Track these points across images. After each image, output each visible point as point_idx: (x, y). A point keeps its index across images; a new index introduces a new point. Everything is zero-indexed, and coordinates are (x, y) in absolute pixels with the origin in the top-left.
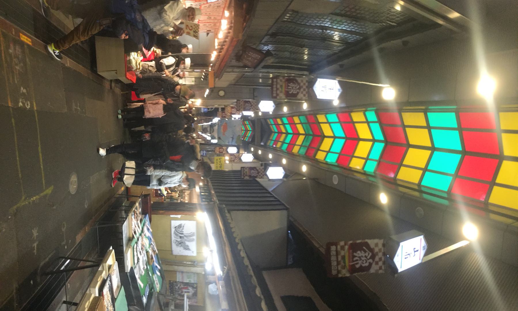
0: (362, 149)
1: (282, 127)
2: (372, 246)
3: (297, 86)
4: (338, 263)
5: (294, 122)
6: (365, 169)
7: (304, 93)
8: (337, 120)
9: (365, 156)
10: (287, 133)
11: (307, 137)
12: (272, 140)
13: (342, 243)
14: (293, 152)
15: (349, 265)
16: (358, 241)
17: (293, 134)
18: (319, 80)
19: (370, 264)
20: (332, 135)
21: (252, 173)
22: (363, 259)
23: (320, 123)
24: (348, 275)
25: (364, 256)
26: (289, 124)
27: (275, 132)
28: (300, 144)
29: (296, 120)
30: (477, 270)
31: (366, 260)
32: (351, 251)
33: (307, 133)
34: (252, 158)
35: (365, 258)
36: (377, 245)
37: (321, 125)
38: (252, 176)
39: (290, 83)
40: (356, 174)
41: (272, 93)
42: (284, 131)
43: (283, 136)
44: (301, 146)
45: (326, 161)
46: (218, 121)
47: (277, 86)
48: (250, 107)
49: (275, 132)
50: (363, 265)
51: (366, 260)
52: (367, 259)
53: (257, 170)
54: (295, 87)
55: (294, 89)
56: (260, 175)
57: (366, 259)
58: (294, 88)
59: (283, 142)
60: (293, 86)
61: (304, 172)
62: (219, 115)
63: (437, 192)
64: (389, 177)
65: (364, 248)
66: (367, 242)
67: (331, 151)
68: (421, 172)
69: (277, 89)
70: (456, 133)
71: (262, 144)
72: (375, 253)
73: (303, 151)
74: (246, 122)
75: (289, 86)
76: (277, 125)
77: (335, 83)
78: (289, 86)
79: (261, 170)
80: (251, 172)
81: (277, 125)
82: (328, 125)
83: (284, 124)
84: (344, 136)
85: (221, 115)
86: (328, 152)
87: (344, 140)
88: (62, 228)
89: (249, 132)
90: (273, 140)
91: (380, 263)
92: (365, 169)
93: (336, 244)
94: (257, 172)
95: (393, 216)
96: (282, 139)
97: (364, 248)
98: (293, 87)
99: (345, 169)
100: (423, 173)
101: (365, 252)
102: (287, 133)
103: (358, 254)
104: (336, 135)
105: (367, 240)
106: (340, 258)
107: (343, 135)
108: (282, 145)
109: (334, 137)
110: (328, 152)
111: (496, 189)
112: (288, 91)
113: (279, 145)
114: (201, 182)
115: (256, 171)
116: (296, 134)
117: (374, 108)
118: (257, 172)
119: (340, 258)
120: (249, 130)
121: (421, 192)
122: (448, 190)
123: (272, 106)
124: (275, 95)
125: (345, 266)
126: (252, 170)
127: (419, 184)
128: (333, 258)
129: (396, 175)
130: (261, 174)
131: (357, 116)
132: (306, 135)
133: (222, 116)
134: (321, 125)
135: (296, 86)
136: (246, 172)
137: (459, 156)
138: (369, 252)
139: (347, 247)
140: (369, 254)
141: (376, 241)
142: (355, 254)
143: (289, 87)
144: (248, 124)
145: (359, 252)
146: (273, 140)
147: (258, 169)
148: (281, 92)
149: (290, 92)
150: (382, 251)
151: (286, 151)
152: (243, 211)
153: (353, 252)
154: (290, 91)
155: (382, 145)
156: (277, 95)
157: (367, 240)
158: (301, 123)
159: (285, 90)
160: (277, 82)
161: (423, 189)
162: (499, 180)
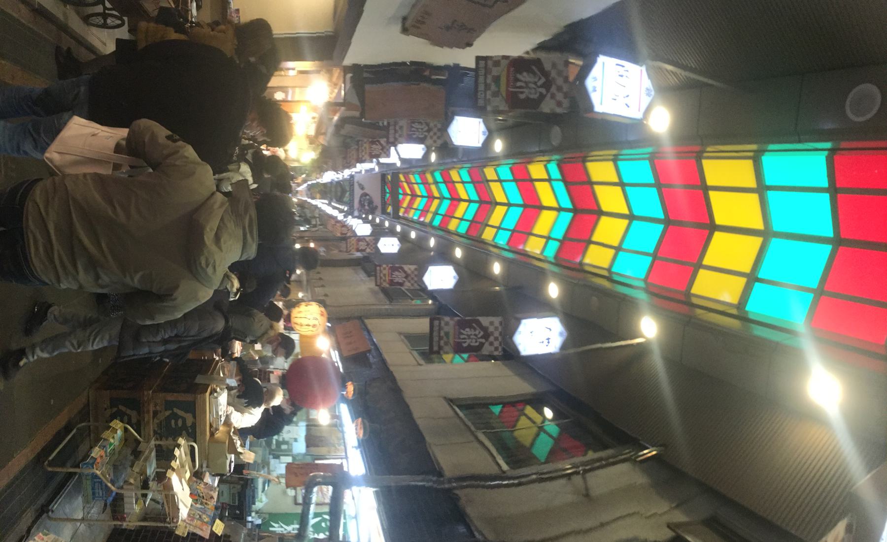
0: (545, 223)
1: (433, 187)
4: (440, 338)
5: (529, 175)
6: (545, 254)
7: (435, 138)
8: (512, 178)
9: (616, 243)
10: (442, 198)
12: (403, 207)
13: (384, 266)
15: (455, 341)
16: (397, 265)
18: (602, 59)
19: (482, 344)
20: (626, 211)
21: (466, 337)
22: (472, 337)
23: (488, 181)
24: (388, 286)
26: (445, 182)
27: (408, 195)
29: (490, 173)
30: (840, 471)
32: (390, 271)
34: (454, 277)
35: (475, 337)
37: (653, 182)
38: (395, 281)
39: (521, 73)
40: (699, 311)
41: (476, 99)
42: (436, 194)
43: (436, 202)
47: (439, 333)
48: (426, 134)
49: (348, 191)
50: (472, 344)
53: (546, 74)
54: (422, 129)
56: (553, 96)
59: (436, 213)
61: (497, 275)
62: (350, 157)
63: (706, 301)
64: (520, 249)
65: (474, 325)
66: (478, 320)
68: (743, 281)
69: (396, 131)
70: (654, 191)
74: (414, 177)
75: (413, 127)
77: (480, 122)
79: (496, 328)
80: (517, 80)
82: (498, 184)
83: (436, 183)
84: (661, 216)
85: (368, 151)
86: (618, 249)
87: (521, 210)
89: (498, 207)
90: (419, 210)
91: (496, 344)
92: (545, 254)
93: (380, 266)
94: (404, 275)
96: (433, 208)
97: (474, 325)
99: (477, 241)
102: (442, 198)
104: (512, 202)
106: (442, 334)
107: (521, 202)
108: (433, 219)
111: (702, 273)
112: (516, 92)
115: (403, 273)
116: (456, 200)
117: (469, 165)
118: (404, 275)
119: (442, 334)
120: (419, 194)
121: (609, 279)
122: (740, 303)
123: (421, 150)
124: (481, 102)
127: (609, 270)
129: (425, 219)
130: (496, 339)
131: (536, 170)
133: (370, 153)
136: (447, 334)
137: (660, 227)
140: (480, 333)
141: (491, 319)
142: (519, 76)
144: (419, 181)
146: (419, 210)
148: (496, 94)
149: (522, 96)
150: (500, 330)
151: (506, 247)
152: (409, 404)
154: (465, 342)
155: (520, 210)
157: (403, 266)
159: (507, 90)
161: (695, 301)
162: (706, 261)
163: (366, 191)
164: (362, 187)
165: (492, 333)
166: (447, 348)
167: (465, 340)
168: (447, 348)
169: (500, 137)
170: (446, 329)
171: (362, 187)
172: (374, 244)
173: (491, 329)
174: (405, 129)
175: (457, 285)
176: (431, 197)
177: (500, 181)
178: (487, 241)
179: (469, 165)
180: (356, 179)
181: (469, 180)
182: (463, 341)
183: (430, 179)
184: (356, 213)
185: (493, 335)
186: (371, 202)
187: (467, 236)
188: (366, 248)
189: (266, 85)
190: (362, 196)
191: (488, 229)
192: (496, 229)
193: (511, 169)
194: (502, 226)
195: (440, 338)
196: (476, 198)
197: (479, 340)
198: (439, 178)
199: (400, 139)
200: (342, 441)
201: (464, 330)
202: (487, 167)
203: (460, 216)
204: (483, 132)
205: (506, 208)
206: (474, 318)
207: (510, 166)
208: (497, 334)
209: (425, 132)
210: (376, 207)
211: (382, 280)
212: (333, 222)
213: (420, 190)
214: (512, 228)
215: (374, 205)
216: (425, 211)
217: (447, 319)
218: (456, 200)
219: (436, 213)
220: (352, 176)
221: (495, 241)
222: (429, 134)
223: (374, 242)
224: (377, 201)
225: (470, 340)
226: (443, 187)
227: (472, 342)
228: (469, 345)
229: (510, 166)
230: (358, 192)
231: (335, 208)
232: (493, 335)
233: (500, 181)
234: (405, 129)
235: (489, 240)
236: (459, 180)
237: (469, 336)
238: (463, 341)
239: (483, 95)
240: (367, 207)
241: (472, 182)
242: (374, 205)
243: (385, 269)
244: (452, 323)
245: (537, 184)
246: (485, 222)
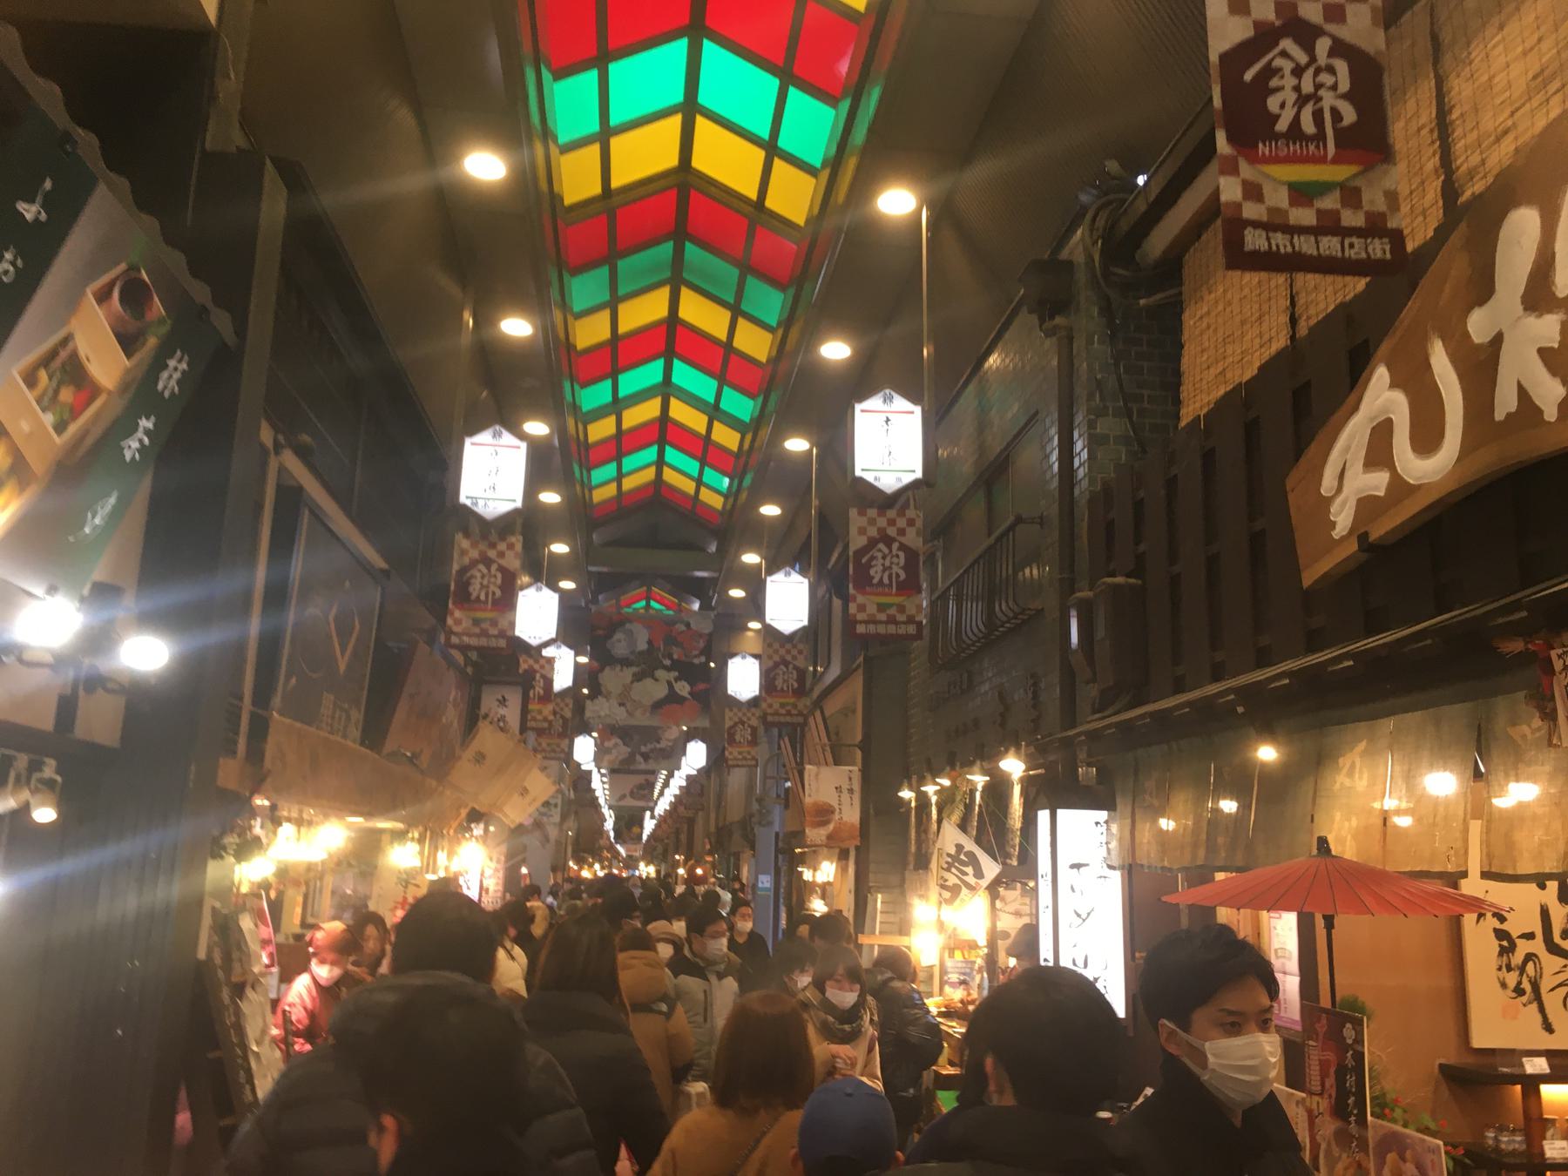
2: (731, 723)
3: (480, 571)
8: (592, 76)
10: (666, 389)
11: (685, 275)
14: (751, 419)
17: (669, 355)
20: (676, 121)
25: (1294, 81)
28: (725, 316)
31: (1317, 72)
32: (1263, 149)
33: (667, 274)
35: (888, 558)
36: (731, 719)
37: (616, 183)
43: (680, 412)
44: (736, 311)
45: (825, 164)
46: (601, 681)
47: (881, 622)
50: (1345, 85)
51: (1317, 72)
52: (1308, 66)
53: (776, 665)
54: (483, 577)
55: (489, 582)
56: (902, 532)
57: (1311, 71)
58: (485, 582)
59: (714, 412)
60: (478, 586)
65: (864, 561)
67: (765, 134)
71: (713, 548)
72: (1278, 23)
73: (769, 302)
75: (478, 597)
76: (622, 444)
78: (478, 597)
79: (872, 522)
81: (622, 444)
82: (616, 143)
83: (617, 405)
84: (680, 47)
86: (771, 148)
87: (709, 48)
88: (455, 825)
89: (698, 163)
90: (701, 473)
95: (965, 157)
96: (696, 421)
97: (864, 561)
98: (481, 584)
100: (705, 403)
101: (873, 558)
102: (666, 389)
103: (1283, 106)
104: (678, 96)
105: (1214, 57)
106: (883, 617)
108: (733, 422)
109: (690, 109)
110: (771, 148)
113: (726, 437)
114: (1256, 750)
119: (883, 617)
125: (1342, 186)
126: (1273, 103)
128: (881, 629)
130: (892, 522)
132: (676, 280)
134: (616, 183)
135: (479, 575)
136: (881, 608)
138: (1276, 51)
139: (1246, 170)
143: (483, 597)
145: (872, 572)
146: (701, 473)
147: (770, 664)
151: (845, 105)
153: (776, 690)
156: (545, 719)
157: (1214, 57)
158: (613, 305)
159: (491, 610)
160: (866, 622)
163: (627, 792)
164: (623, 797)
165: (882, 531)
166: (1373, 199)
167: (894, 576)
168: (1373, 199)
169: (457, 158)
170: (872, 609)
171: (623, 797)
172: (740, 710)
173: (873, 532)
174: (480, 615)
175: (703, 741)
176: (664, 432)
177: (605, 134)
178: (756, 414)
179: (567, 385)
180: (614, 803)
181: (608, 383)
182: (894, 580)
183: (602, 430)
184: (652, 804)
185: (885, 529)
186: (641, 787)
187: (736, 474)
188: (902, 547)
189: (591, 880)
190: (634, 798)
191: (715, 436)
192: (777, 162)
193: (584, 385)
194: (764, 133)
195: (745, 759)
196: (667, 248)
197: (894, 552)
198: (609, 470)
199: (503, 624)
200: (780, 844)
201: (873, 578)
202: (577, 403)
203: (705, 479)
204: (494, 436)
205: (700, 120)
206: (1215, 72)
207: (576, 387)
208: (882, 522)
209: (489, 571)
210: (646, 780)
211: (749, 757)
212: (681, 809)
213: (639, 464)
214: (774, 83)
215: (643, 782)
216: (703, 449)
217: (727, 753)
218: (664, 432)
219: (714, 412)
220: (610, 808)
221: (818, 163)
222: (494, 561)
223: (735, 710)
224: (640, 779)
225: (894, 566)
226: (630, 462)
227: (898, 564)
228: (796, 681)
229: (576, 387)
230: (630, 802)
231: (661, 794)
232: (885, 529)
233: (605, 134)
234: (480, 615)
235: (755, 407)
236: (614, 485)
237: (784, 681)
238: (894, 580)
239: (1355, 240)
240: (646, 792)
241: (614, 375)
242: (643, 782)
243: (1253, 192)
244: (860, 599)
245: (622, 329)
246: (749, 209)
